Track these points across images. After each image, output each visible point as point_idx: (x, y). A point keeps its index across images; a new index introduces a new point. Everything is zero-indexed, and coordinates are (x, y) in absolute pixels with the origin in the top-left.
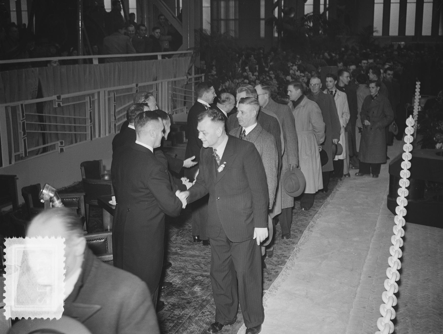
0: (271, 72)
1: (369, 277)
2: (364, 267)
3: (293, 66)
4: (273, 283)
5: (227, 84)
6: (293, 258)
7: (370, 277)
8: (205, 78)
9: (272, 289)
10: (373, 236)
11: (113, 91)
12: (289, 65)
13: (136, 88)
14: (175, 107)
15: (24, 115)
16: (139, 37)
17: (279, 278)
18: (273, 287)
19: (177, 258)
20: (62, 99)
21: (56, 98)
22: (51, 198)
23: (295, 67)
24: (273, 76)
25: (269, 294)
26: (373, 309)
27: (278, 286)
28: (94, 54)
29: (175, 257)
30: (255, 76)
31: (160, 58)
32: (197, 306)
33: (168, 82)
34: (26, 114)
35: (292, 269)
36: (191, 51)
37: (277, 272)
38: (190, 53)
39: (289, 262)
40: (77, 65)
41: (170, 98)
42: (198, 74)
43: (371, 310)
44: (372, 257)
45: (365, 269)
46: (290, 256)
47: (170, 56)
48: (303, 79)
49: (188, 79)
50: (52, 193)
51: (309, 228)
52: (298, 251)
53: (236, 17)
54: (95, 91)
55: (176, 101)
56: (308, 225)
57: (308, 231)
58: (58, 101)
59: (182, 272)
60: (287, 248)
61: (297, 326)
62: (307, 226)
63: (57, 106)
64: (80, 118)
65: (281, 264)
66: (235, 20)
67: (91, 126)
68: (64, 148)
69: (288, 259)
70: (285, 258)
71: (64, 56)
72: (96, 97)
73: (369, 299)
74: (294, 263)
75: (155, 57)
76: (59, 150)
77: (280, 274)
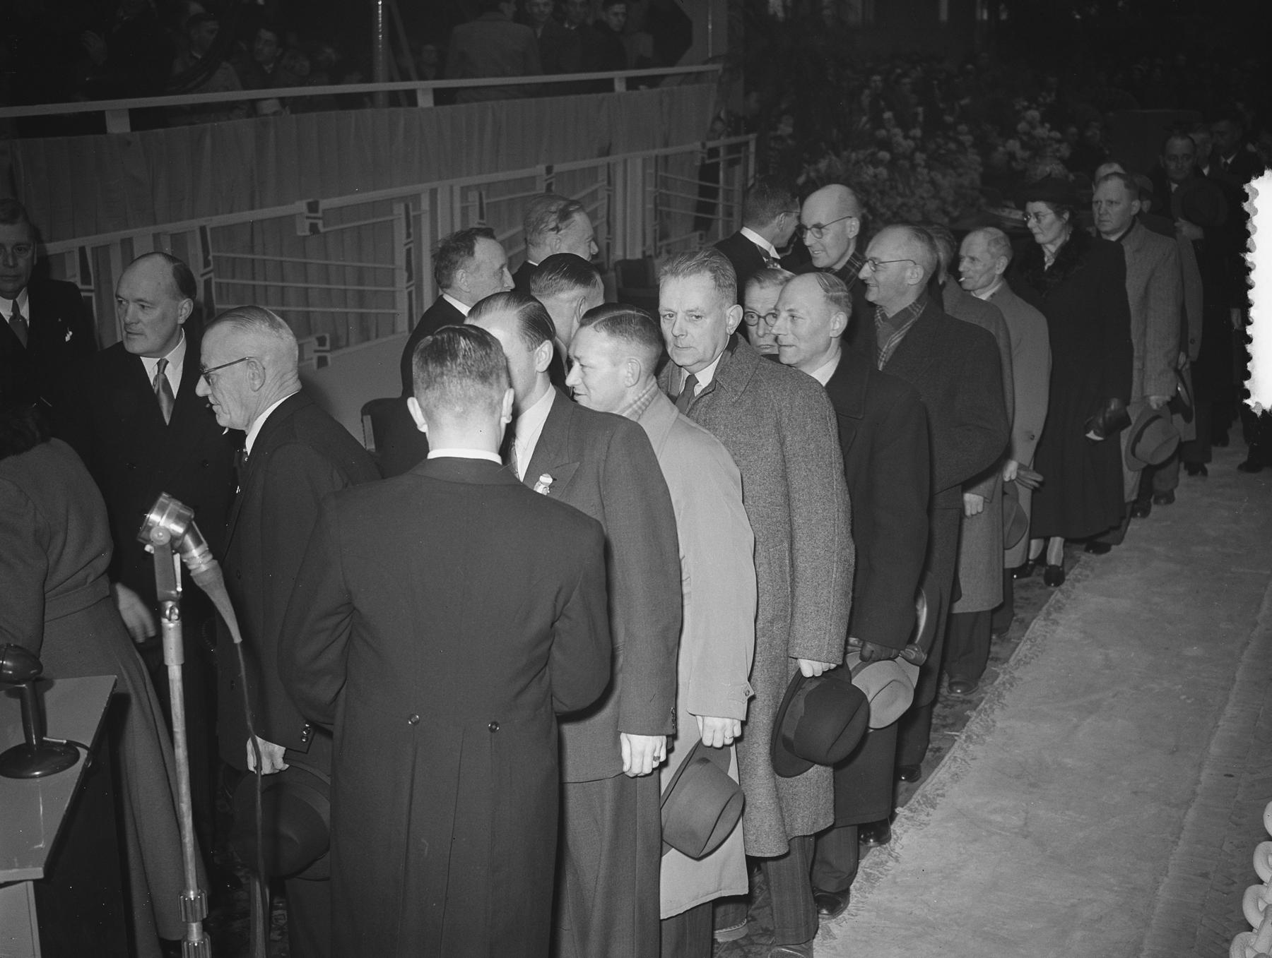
0: (963, 128)
1: (1226, 775)
2: (1213, 742)
3: (1028, 108)
4: (922, 787)
5: (823, 165)
6: (991, 707)
7: (1231, 776)
9: (917, 806)
10: (1248, 643)
11: (478, 187)
12: (1018, 107)
13: (545, 177)
14: (663, 235)
15: (210, 258)
16: (567, 26)
17: (943, 770)
18: (922, 796)
20: (324, 211)
21: (544, 171)
22: (174, 538)
23: (1034, 114)
24: (968, 139)
25: (907, 818)
26: (1234, 882)
27: (938, 795)
28: (422, 77)
31: (620, 87)
33: (644, 160)
34: (214, 257)
35: (984, 741)
36: (718, 67)
37: (939, 749)
39: (976, 717)
40: (368, 112)
41: (650, 206)
42: (736, 133)
43: (1227, 885)
44: (1242, 711)
45: (1214, 749)
46: (981, 701)
47: (653, 82)
48: (1058, 150)
49: (706, 151)
50: (177, 523)
51: (1049, 613)
52: (1008, 686)
54: (423, 188)
55: (668, 214)
56: (1047, 601)
57: (1043, 623)
58: (315, 218)
60: (1027, 599)
61: (986, 929)
62: (1042, 606)
63: (308, 233)
64: (375, 268)
65: (953, 724)
67: (409, 289)
68: (329, 356)
69: (975, 709)
70: (965, 706)
71: (350, 82)
72: (425, 204)
73: (1221, 848)
74: (994, 722)
75: (608, 85)
76: (315, 362)
77: (946, 758)
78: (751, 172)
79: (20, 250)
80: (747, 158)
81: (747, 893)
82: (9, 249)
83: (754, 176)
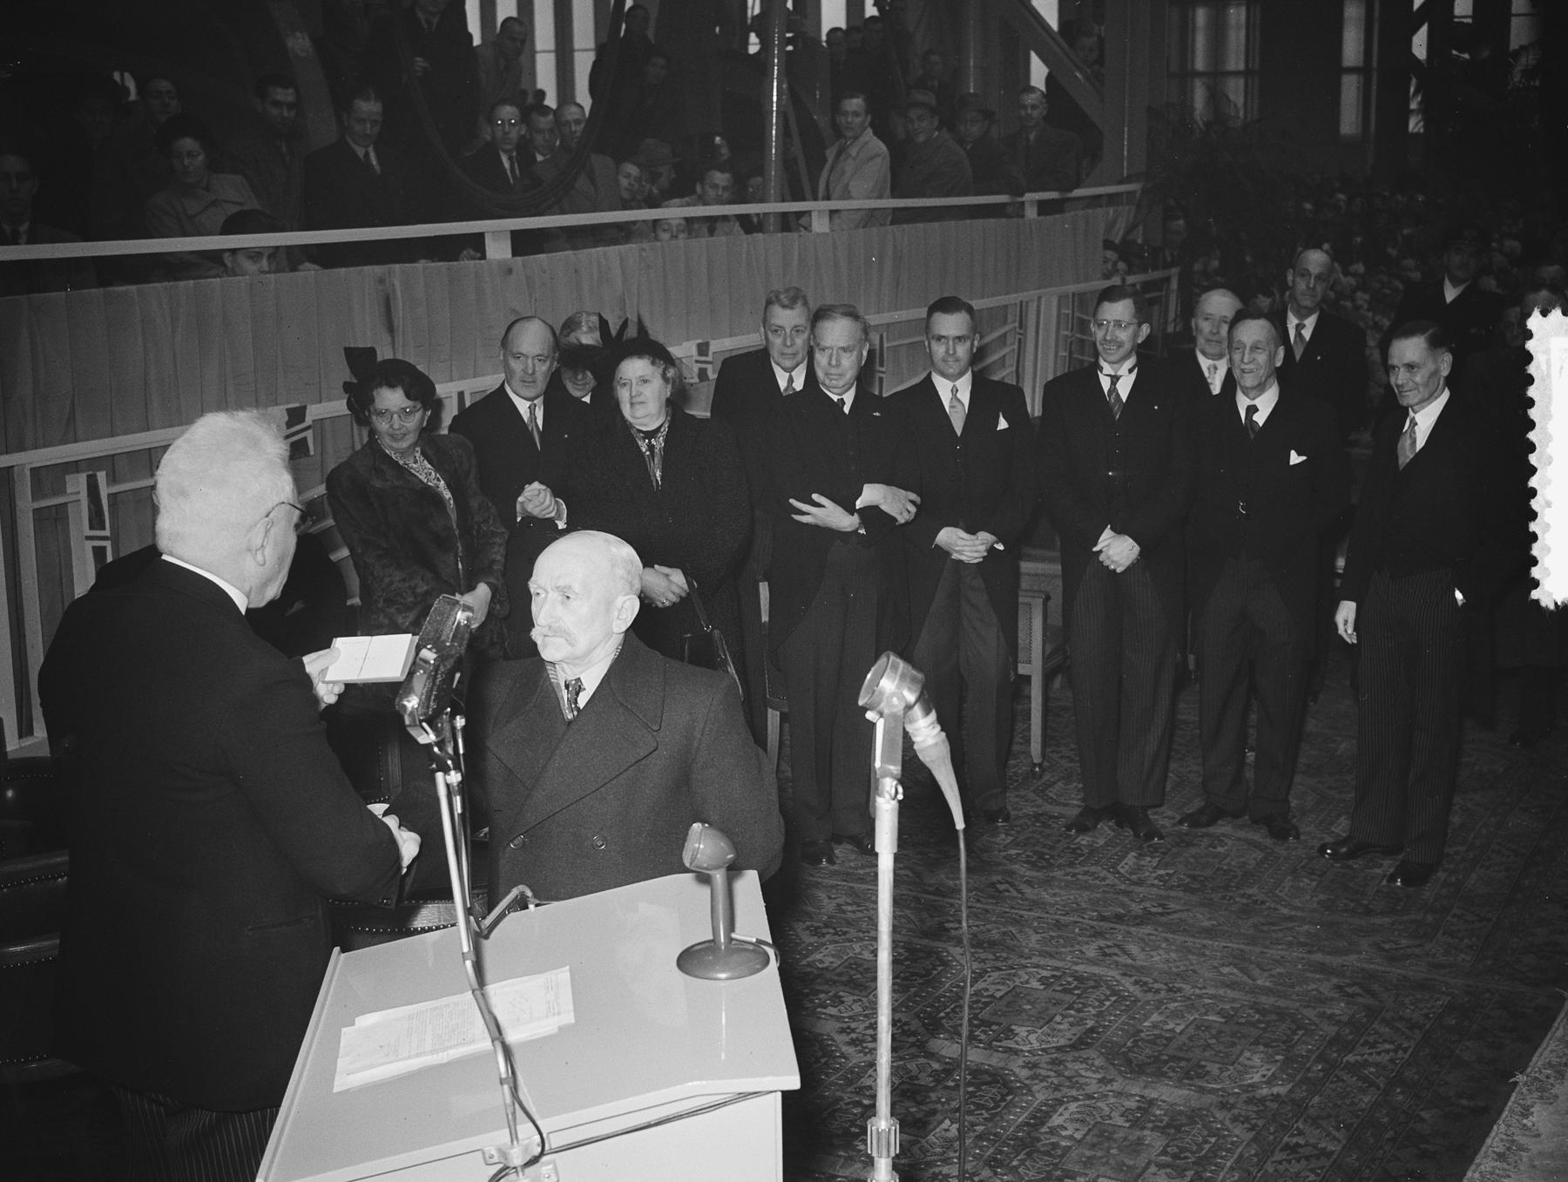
8: (1179, 285)
19: (1153, 937)
21: (694, 351)
29: (1147, 931)
30: (1354, 275)
32: (1260, 1123)
38: (1129, 193)
53: (1250, 66)
59: (1180, 990)
66: (1247, 73)
78: (1172, 315)
79: (798, 331)
80: (1167, 296)
81: (344, 1030)
82: (788, 331)
83: (1175, 320)
